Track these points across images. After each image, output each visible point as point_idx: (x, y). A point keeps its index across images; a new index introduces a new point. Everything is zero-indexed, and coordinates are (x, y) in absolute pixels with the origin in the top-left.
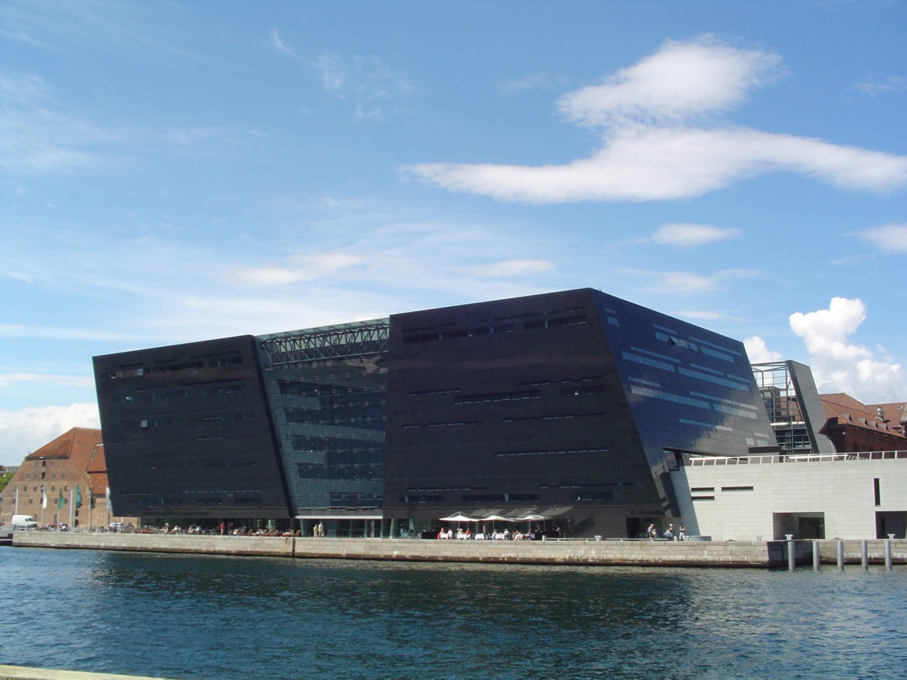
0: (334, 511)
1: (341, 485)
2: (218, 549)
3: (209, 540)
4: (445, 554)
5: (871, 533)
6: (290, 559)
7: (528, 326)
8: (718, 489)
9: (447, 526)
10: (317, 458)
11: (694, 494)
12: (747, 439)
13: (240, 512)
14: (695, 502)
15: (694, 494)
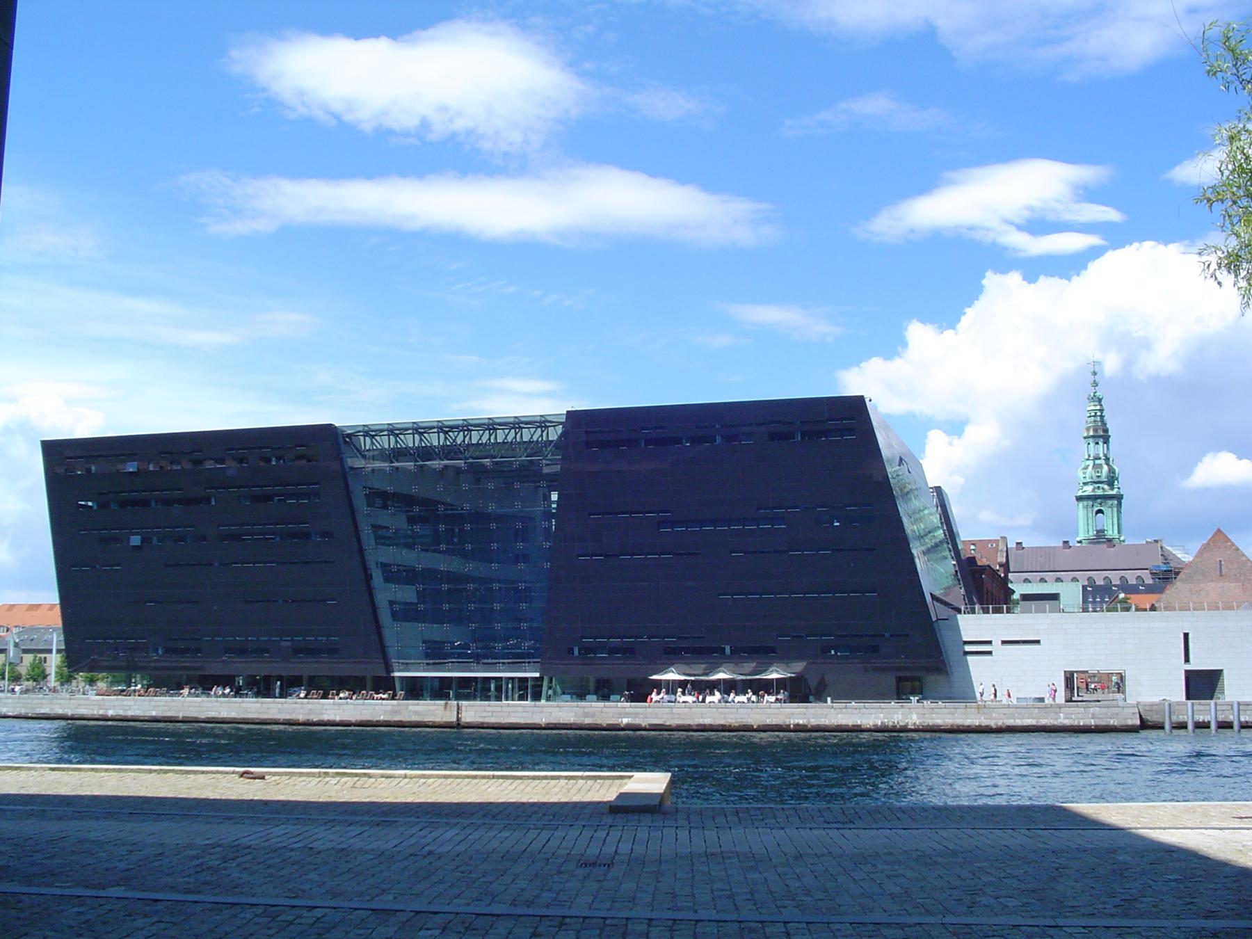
0: (429, 667)
1: (435, 631)
2: (326, 718)
3: (310, 706)
4: (701, 721)
5: (1177, 692)
7: (773, 436)
9: (658, 685)
10: (407, 594)
11: (968, 648)
12: (132, 544)
13: (306, 667)
14: (969, 658)
15: (968, 648)
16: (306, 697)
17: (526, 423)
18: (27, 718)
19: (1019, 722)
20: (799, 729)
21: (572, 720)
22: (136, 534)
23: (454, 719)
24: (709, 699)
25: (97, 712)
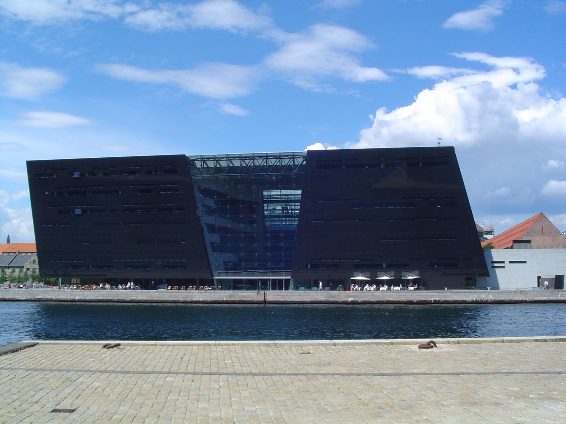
2: (195, 299)
3: (186, 294)
6: (262, 305)
8: (507, 262)
9: (356, 282)
11: (496, 265)
14: (496, 269)
15: (496, 265)
16: (171, 289)
17: (271, 156)
18: (516, 302)
19: (540, 299)
20: (436, 302)
21: (323, 299)
22: (79, 208)
23: (263, 300)
24: (381, 289)
25: (69, 297)
